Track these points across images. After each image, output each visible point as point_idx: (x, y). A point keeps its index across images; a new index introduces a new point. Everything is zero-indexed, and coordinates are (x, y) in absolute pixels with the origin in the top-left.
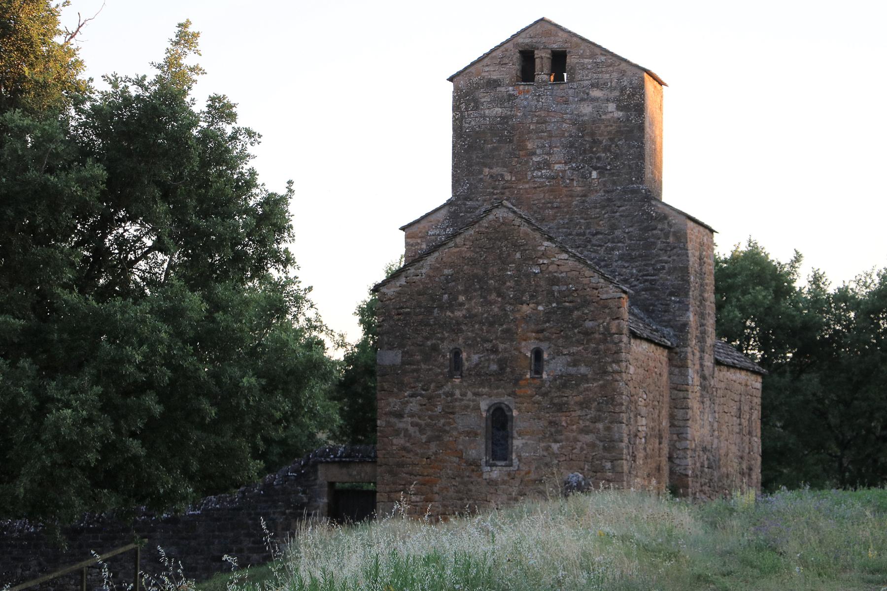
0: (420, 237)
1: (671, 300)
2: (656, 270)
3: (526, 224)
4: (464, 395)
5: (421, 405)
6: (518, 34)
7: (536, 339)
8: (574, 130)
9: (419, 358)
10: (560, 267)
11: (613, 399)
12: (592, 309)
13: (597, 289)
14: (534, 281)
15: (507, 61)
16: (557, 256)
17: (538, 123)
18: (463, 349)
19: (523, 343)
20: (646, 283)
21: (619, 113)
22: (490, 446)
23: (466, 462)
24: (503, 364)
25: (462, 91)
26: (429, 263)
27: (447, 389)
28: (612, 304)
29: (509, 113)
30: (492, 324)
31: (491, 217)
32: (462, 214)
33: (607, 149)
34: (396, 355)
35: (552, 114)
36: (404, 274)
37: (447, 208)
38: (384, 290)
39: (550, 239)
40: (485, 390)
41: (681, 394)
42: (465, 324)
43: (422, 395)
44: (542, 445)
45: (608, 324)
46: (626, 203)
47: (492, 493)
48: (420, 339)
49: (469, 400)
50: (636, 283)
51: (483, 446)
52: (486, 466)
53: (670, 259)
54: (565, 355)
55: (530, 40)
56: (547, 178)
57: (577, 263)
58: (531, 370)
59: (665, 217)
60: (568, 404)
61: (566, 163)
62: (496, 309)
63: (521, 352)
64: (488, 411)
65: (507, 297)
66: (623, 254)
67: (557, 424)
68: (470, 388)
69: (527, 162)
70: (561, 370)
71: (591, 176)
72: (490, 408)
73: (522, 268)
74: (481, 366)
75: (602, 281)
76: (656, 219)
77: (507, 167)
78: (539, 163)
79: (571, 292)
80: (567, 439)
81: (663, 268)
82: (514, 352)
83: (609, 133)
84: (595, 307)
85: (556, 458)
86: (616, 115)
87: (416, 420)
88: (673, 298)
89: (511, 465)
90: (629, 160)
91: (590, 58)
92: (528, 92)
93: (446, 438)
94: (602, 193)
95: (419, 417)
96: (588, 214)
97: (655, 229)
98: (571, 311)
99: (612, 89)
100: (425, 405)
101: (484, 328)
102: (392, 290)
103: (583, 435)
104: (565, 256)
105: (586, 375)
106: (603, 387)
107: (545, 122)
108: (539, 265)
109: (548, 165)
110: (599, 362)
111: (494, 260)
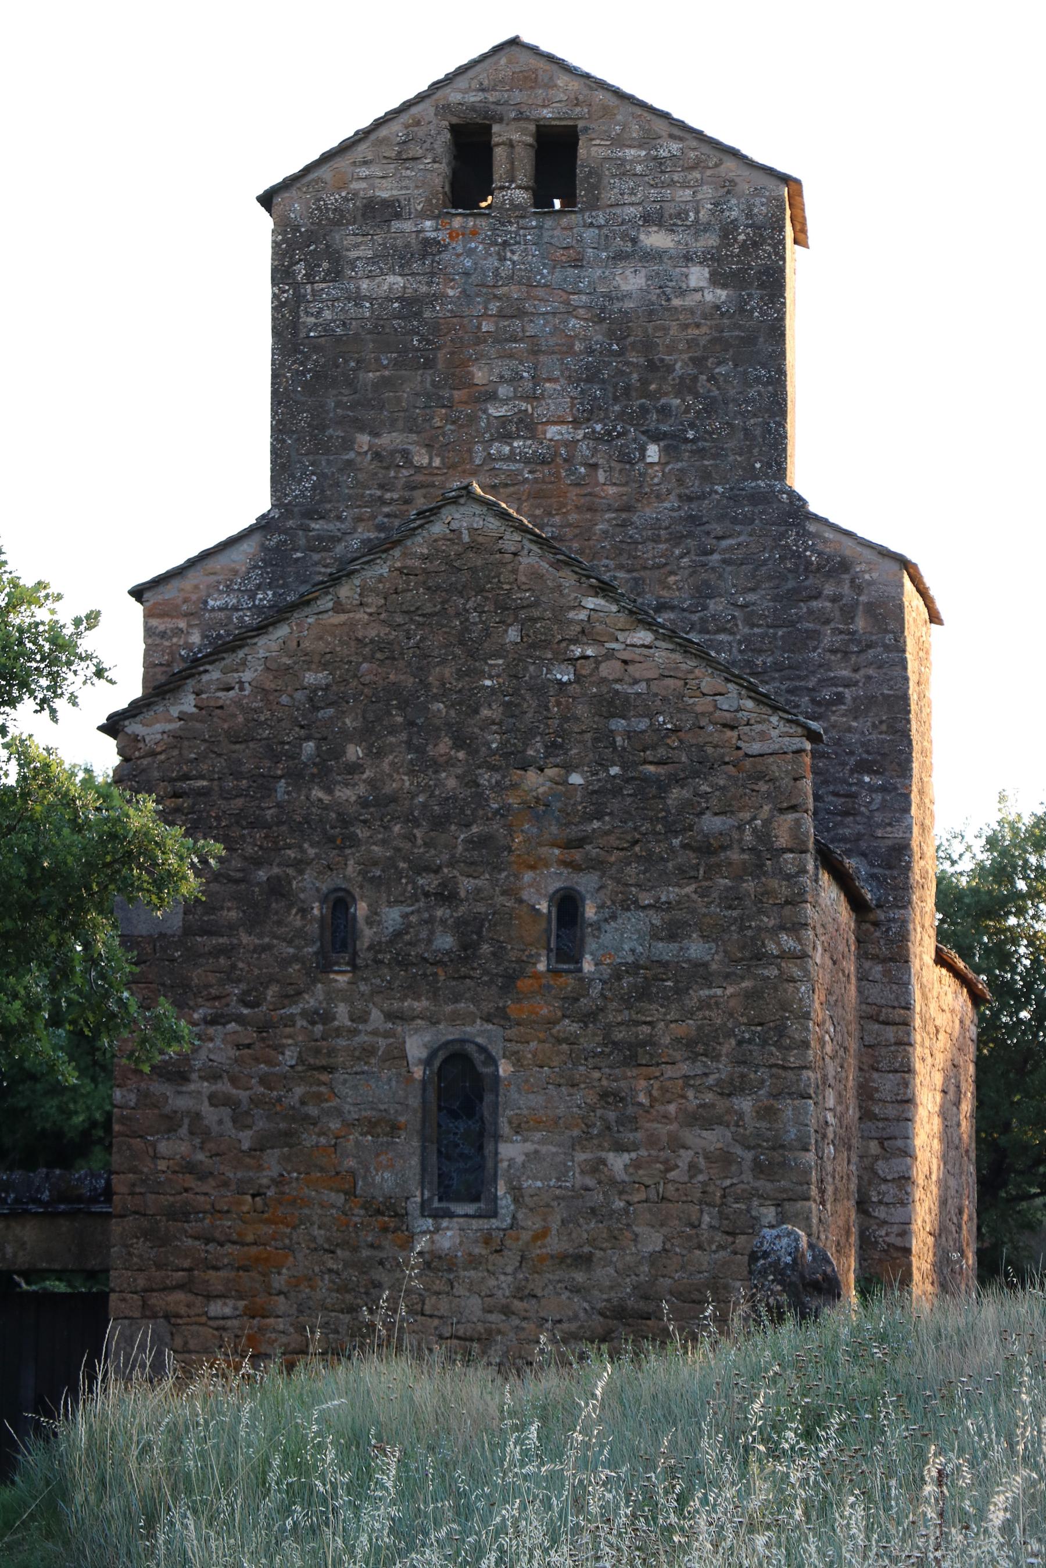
1: (860, 783)
2: (819, 704)
4: (362, 1018)
5: (238, 1047)
6: (449, 79)
8: (597, 336)
9: (233, 914)
10: (631, 668)
11: (781, 1030)
12: (722, 783)
13: (733, 728)
14: (558, 704)
15: (420, 152)
16: (621, 636)
18: (356, 892)
19: (528, 876)
21: (719, 291)
22: (434, 1159)
23: (365, 1206)
25: (296, 229)
26: (262, 654)
27: (312, 1002)
28: (776, 767)
29: (424, 289)
30: (439, 823)
31: (437, 529)
32: (299, 555)
33: (686, 387)
35: (541, 292)
37: (257, 538)
38: (134, 727)
39: (604, 589)
40: (421, 1005)
41: (890, 1033)
42: (365, 822)
43: (240, 1019)
44: (581, 1156)
45: (767, 823)
46: (738, 528)
47: (438, 1293)
49: (375, 1033)
51: (415, 1161)
52: (423, 1216)
55: (480, 96)
56: (527, 461)
57: (678, 657)
58: (550, 950)
59: (844, 566)
60: (653, 1044)
61: (576, 423)
62: (452, 783)
63: (521, 901)
64: (428, 1062)
67: (622, 1099)
69: (473, 419)
71: (643, 456)
73: (526, 669)
74: (407, 937)
75: (749, 704)
76: (818, 570)
77: (418, 433)
78: (504, 420)
79: (662, 735)
80: (652, 1141)
81: (840, 699)
82: (501, 899)
83: (692, 343)
84: (730, 777)
85: (621, 1193)
86: (709, 297)
87: (224, 1087)
88: (867, 779)
91: (640, 146)
92: (474, 233)
93: (310, 1139)
94: (672, 502)
95: (234, 1081)
96: (636, 557)
98: (663, 787)
99: (699, 229)
100: (248, 1046)
101: (418, 833)
102: (159, 727)
104: (643, 636)
105: (705, 965)
106: (752, 996)
107: (520, 314)
108: (573, 661)
109: (528, 426)
110: (742, 929)
111: (446, 646)
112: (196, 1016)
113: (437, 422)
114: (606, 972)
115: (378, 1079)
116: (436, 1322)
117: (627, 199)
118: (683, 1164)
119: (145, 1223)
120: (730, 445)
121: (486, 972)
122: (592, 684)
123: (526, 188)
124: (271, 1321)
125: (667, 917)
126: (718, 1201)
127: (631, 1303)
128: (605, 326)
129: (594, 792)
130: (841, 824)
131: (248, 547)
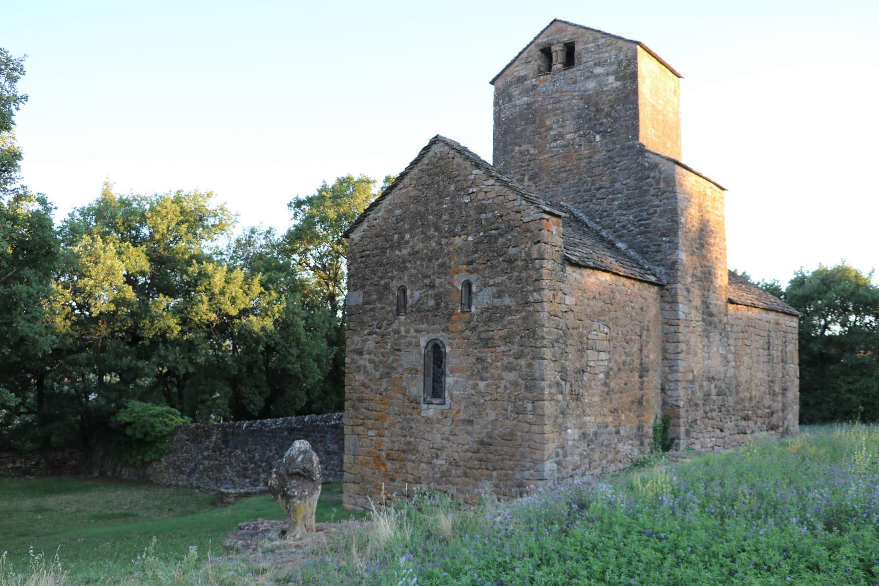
1: (662, 240)
3: (458, 155)
4: (408, 332)
7: (468, 271)
11: (534, 332)
12: (515, 234)
14: (465, 211)
17: (553, 103)
18: (407, 286)
20: (641, 228)
23: (408, 399)
24: (438, 298)
25: (500, 90)
26: (384, 206)
27: (395, 327)
28: (532, 226)
30: (430, 260)
33: (608, 115)
34: (359, 296)
35: (564, 94)
36: (366, 219)
41: (672, 329)
44: (471, 382)
45: (529, 249)
48: (376, 279)
49: (412, 337)
50: (632, 228)
53: (661, 203)
54: (491, 286)
56: (561, 147)
59: (656, 166)
61: (575, 132)
62: (434, 244)
63: (453, 286)
64: (426, 347)
65: (443, 231)
66: (622, 204)
67: (483, 361)
68: (412, 325)
69: (546, 136)
72: (427, 344)
75: (524, 202)
78: (555, 135)
80: (492, 377)
81: (655, 212)
82: (447, 286)
83: (610, 101)
85: (483, 397)
86: (615, 85)
87: (372, 357)
88: (664, 239)
89: (444, 404)
90: (626, 121)
91: (593, 43)
94: (604, 153)
95: (375, 354)
97: (648, 178)
98: (496, 238)
99: (611, 64)
101: (424, 263)
102: (358, 235)
103: (507, 373)
104: (491, 181)
105: (510, 307)
106: (525, 318)
107: (559, 102)
109: (561, 136)
113: (536, 139)
116: (428, 442)
117: (589, 60)
118: (502, 386)
119: (352, 403)
120: (622, 131)
121: (443, 313)
123: (561, 63)
124: (384, 438)
126: (513, 401)
127: (485, 439)
130: (656, 256)
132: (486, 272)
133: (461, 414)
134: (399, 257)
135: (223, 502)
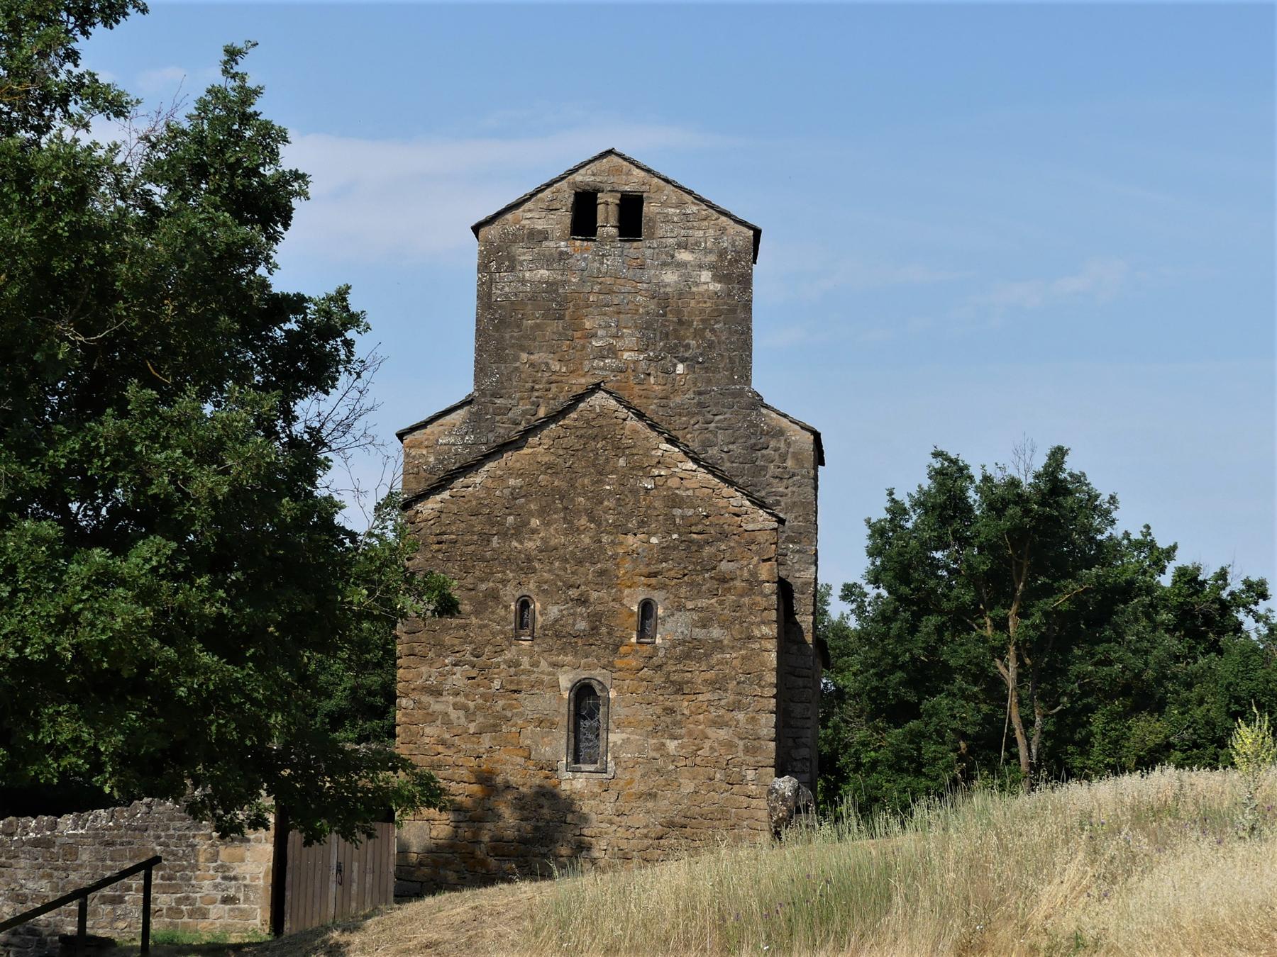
0: (427, 447)
1: (787, 548)
4: (535, 664)
8: (652, 306)
12: (732, 545)
13: (738, 516)
15: (559, 207)
19: (627, 592)
24: (596, 620)
25: (492, 243)
30: (580, 563)
33: (698, 334)
35: (622, 281)
40: (569, 659)
45: (755, 566)
49: (542, 673)
51: (563, 741)
55: (592, 178)
62: (587, 540)
63: (622, 605)
65: (604, 523)
68: (546, 655)
69: (584, 347)
70: (682, 633)
73: (628, 480)
75: (748, 503)
80: (690, 734)
83: (702, 311)
86: (711, 287)
87: (461, 699)
91: (676, 207)
94: (690, 395)
95: (466, 696)
98: (700, 547)
99: (707, 251)
100: (474, 678)
105: (721, 641)
108: (653, 477)
109: (613, 352)
112: (447, 661)
114: (668, 644)
115: (544, 698)
122: (664, 490)
125: (701, 615)
127: (677, 819)
128: (656, 300)
129: (663, 548)
131: (461, 413)
132: (683, 590)
133: (635, 785)
134: (520, 552)
135: (1061, 764)
